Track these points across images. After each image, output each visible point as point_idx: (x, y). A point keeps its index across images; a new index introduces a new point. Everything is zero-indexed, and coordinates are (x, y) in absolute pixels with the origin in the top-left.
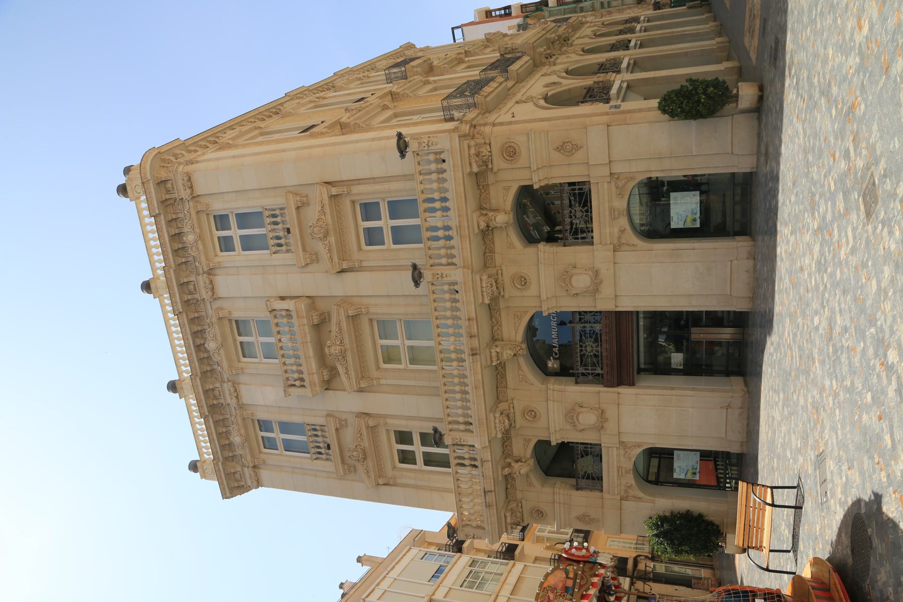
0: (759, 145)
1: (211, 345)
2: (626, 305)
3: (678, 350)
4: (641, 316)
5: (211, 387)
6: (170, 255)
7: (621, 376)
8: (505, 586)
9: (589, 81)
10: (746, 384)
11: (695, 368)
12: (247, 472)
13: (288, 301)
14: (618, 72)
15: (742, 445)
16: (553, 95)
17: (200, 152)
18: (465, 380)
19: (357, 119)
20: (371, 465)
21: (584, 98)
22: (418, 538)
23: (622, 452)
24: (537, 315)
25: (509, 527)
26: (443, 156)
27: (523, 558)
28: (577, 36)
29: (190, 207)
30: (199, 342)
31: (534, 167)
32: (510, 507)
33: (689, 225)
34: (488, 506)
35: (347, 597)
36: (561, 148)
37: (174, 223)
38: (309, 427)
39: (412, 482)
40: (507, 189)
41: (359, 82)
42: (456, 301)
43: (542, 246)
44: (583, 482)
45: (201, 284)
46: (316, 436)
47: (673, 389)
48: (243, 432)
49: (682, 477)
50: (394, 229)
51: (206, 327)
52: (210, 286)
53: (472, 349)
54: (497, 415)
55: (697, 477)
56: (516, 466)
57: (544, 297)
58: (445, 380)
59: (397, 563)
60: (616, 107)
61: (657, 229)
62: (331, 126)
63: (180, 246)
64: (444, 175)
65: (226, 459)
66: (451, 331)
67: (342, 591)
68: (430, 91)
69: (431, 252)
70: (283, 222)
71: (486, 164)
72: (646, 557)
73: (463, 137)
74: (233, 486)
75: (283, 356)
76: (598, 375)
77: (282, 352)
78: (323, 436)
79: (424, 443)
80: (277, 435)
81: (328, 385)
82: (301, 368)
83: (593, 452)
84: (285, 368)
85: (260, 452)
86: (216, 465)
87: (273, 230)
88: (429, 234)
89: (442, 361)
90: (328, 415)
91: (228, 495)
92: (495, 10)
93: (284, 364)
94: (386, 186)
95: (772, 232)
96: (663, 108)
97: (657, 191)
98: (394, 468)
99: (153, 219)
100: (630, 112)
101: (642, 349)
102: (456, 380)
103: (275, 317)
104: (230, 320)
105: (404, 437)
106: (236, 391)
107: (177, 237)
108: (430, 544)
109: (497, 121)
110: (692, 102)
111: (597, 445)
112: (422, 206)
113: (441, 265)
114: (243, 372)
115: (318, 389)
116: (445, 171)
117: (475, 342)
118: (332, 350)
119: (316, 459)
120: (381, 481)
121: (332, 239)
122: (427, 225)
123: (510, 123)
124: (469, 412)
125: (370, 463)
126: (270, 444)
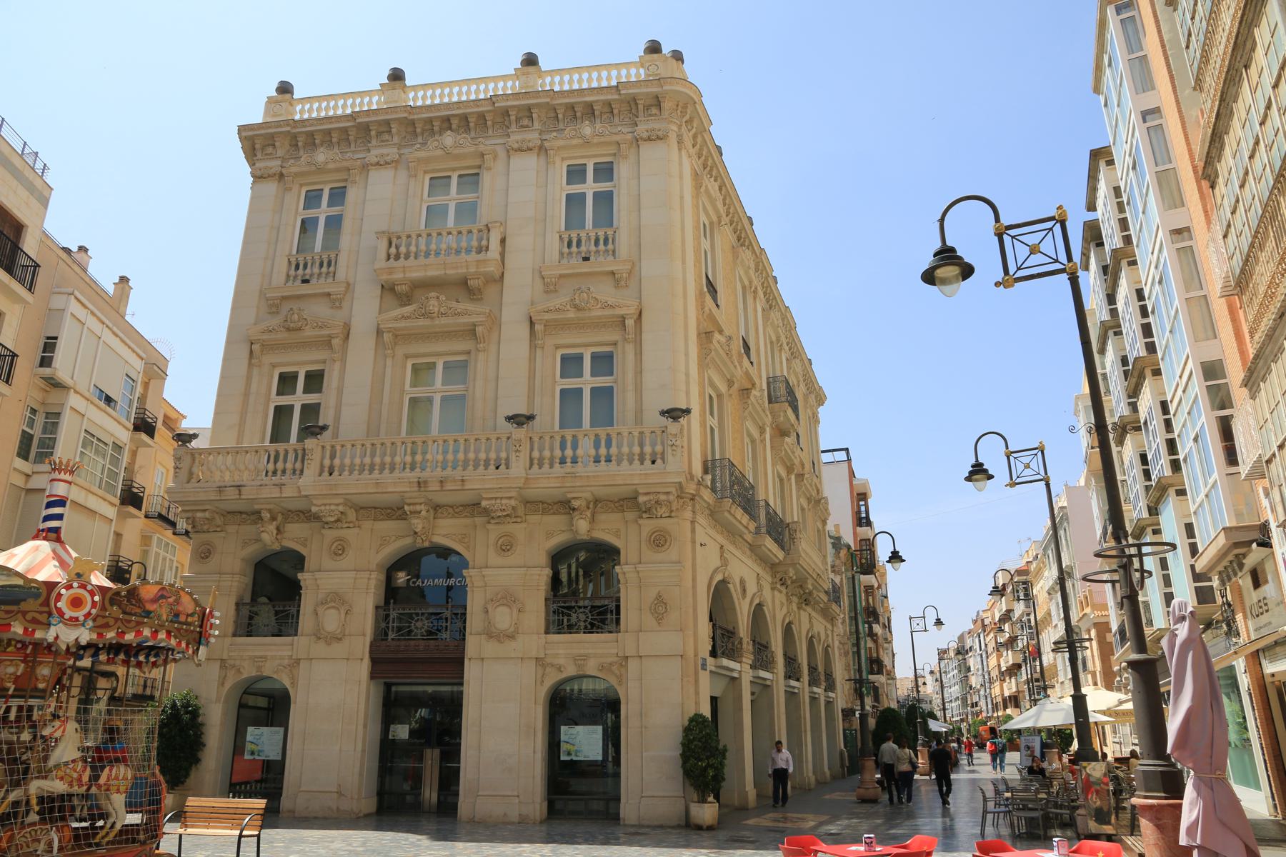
0: (648, 827)
1: (448, 139)
2: (471, 671)
3: (411, 732)
4: (455, 688)
5: (394, 130)
6: (567, 101)
7: (384, 662)
8: (84, 492)
9: (743, 629)
10: (367, 816)
11: (388, 751)
12: (274, 165)
13: (499, 249)
14: (753, 667)
15: (289, 811)
16: (728, 589)
17: (693, 151)
18: (387, 471)
19: (716, 350)
20: (279, 336)
21: (721, 628)
22: (155, 369)
23: (286, 662)
24: (465, 564)
25: (189, 515)
26: (659, 461)
27: (122, 516)
28: (814, 614)
29: (623, 132)
30: (455, 122)
31: (640, 567)
32: (217, 517)
33: (564, 747)
34: (221, 489)
35: (64, 255)
36: (660, 600)
37: (607, 109)
38: (333, 256)
39: (254, 386)
40: (617, 534)
41: (774, 339)
42: (486, 466)
43: (548, 572)
44: (245, 612)
45: (529, 136)
46: (321, 265)
47: (365, 726)
48: (331, 166)
49: (249, 738)
50: (579, 392)
51: (473, 134)
52: (525, 148)
53: (425, 482)
54: (341, 508)
55: (247, 757)
56: (272, 528)
57: (486, 572)
58: (389, 445)
59: (123, 341)
60: (704, 666)
61: (563, 706)
62: (712, 318)
63: (578, 114)
64: (637, 462)
65: (294, 137)
66: (450, 457)
67: (75, 249)
68: (750, 435)
69: (547, 438)
70: (597, 252)
71: (647, 511)
72: (115, 690)
73: (680, 486)
74: (256, 142)
75: (429, 235)
76: (386, 634)
77: (434, 234)
78: (320, 274)
79: (305, 408)
80: (323, 212)
81: (388, 289)
82: (412, 258)
83: (285, 624)
84: (414, 237)
85: (301, 185)
86: (287, 123)
87: (589, 238)
88: (569, 438)
89: (413, 443)
90: (348, 284)
91: (244, 134)
92: (866, 506)
93: (419, 235)
94: (631, 387)
95: (549, 840)
96: (697, 720)
97: (605, 710)
98: (274, 366)
99: (614, 83)
100: (697, 681)
101: (420, 688)
102: (388, 459)
103: (480, 231)
104: (479, 167)
105: (315, 381)
106: (387, 163)
107: (590, 111)
108: (146, 385)
109: (697, 527)
110: (702, 754)
111: (296, 630)
112: (602, 432)
113: (532, 450)
114: (410, 176)
115: (385, 277)
116: (642, 463)
117: (434, 486)
118: (433, 302)
119: (290, 262)
120: (255, 347)
121: (571, 314)
122: (580, 437)
123: (693, 542)
124: (346, 473)
125: (282, 336)
126: (312, 199)
